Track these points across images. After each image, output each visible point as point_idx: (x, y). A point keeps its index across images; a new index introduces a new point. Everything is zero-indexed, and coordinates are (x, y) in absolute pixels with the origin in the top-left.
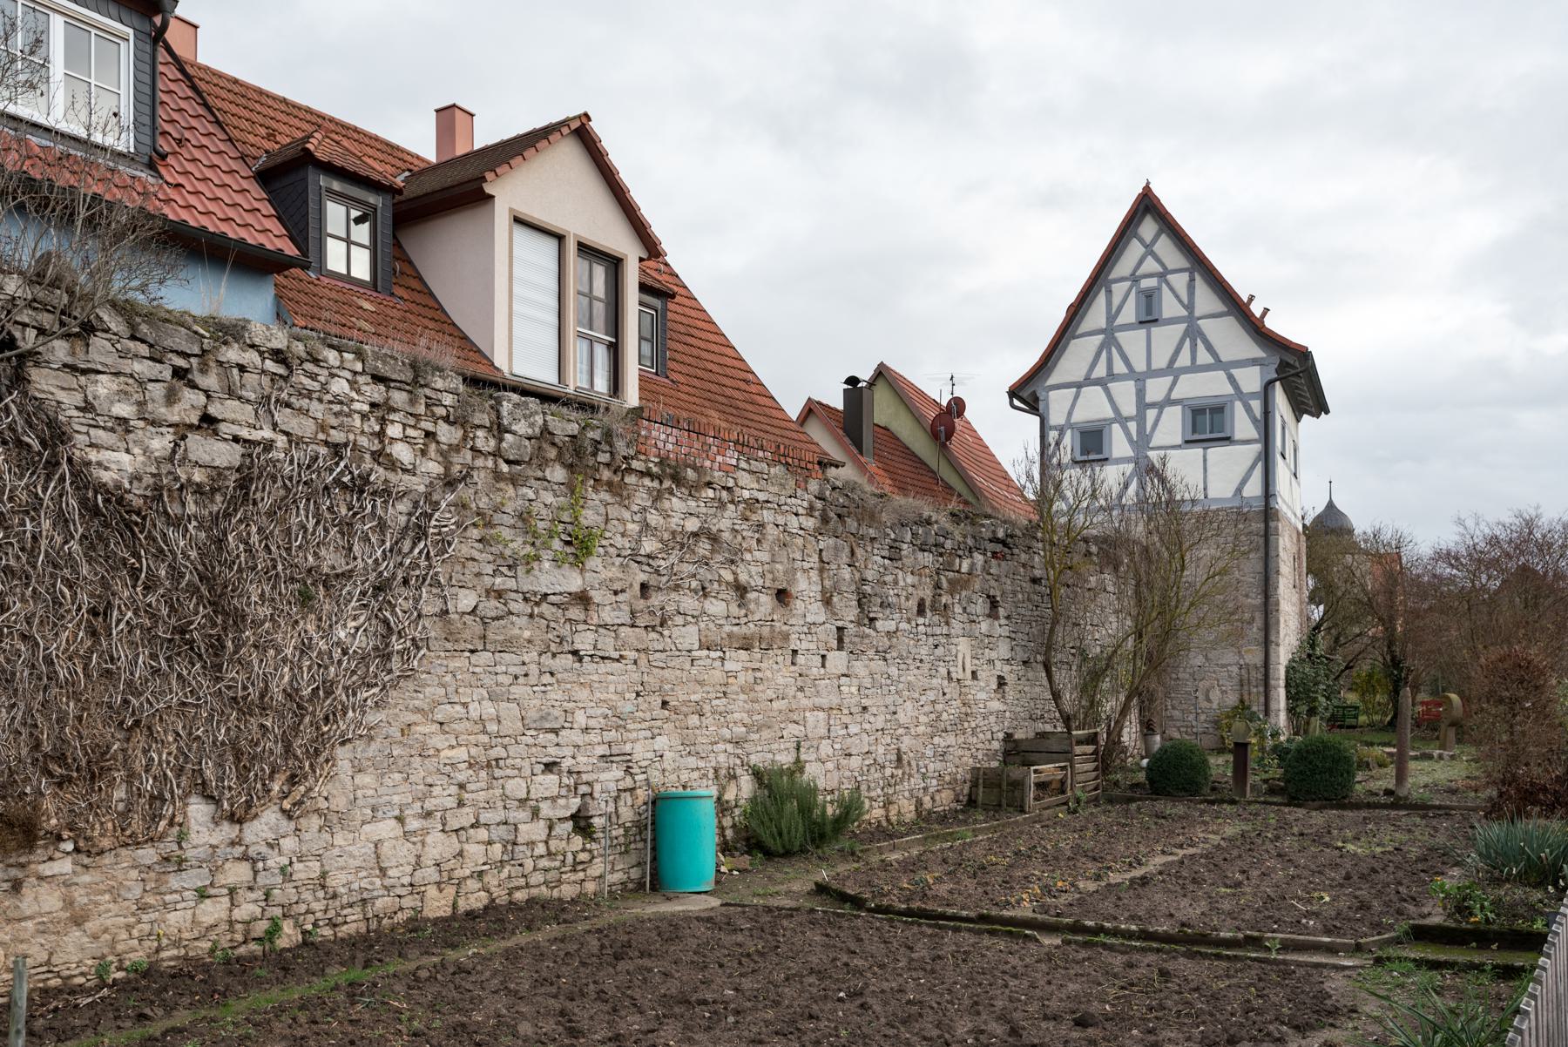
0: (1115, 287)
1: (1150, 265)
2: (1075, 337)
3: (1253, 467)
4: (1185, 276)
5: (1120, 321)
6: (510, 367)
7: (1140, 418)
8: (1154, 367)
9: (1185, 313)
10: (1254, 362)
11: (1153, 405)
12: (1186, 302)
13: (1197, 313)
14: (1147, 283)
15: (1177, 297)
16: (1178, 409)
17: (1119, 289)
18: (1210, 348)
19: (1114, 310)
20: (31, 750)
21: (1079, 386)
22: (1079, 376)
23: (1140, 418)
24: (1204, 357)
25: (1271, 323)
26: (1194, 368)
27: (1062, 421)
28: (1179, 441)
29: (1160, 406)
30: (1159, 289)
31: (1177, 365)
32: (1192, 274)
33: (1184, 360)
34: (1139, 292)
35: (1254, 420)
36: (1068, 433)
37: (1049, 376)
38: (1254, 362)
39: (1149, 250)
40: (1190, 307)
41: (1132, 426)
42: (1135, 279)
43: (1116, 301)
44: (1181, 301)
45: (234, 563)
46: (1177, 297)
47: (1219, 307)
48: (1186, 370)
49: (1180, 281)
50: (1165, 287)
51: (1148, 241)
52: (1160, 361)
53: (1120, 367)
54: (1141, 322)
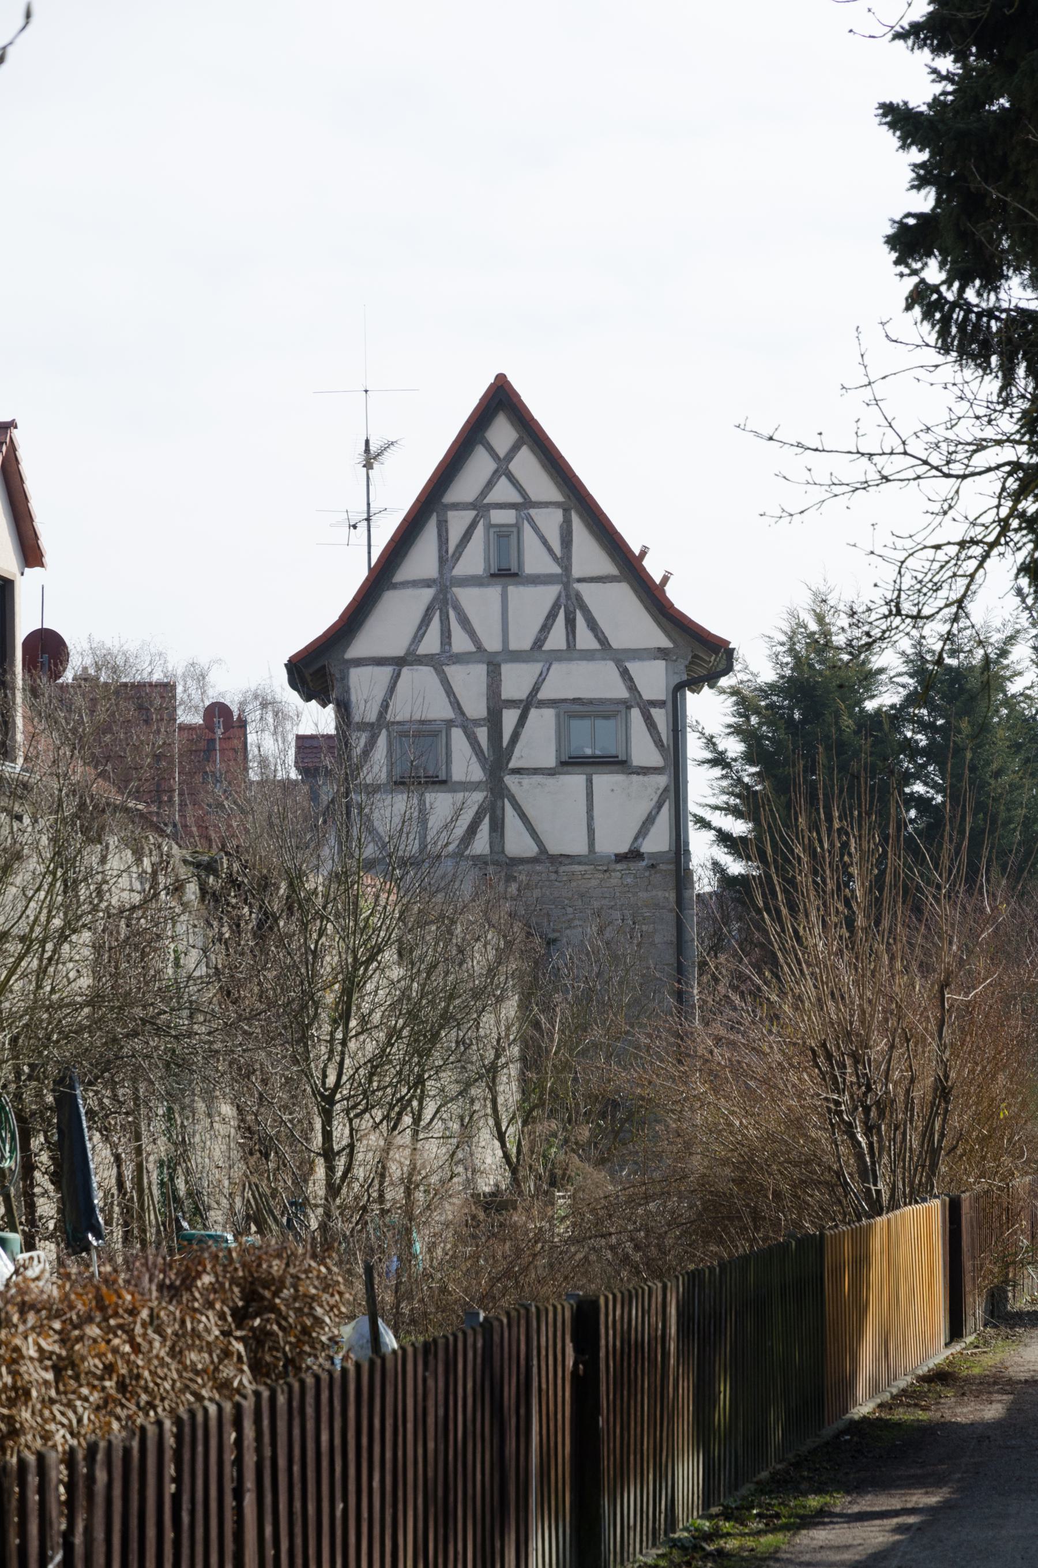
0: (451, 515)
1: (503, 491)
2: (395, 586)
3: (659, 806)
4: (558, 515)
5: (461, 569)
6: (359, 662)
7: (494, 720)
8: (513, 646)
9: (556, 570)
10: (662, 653)
11: (512, 703)
12: (559, 554)
13: (577, 572)
14: (499, 517)
15: (545, 542)
16: (549, 714)
17: (458, 523)
18: (593, 625)
19: (451, 549)
20: (241, 1317)
21: (399, 662)
22: (397, 648)
23: (494, 720)
24: (585, 639)
25: (677, 596)
26: (571, 652)
27: (372, 717)
28: (551, 762)
29: (526, 705)
30: (518, 526)
31: (547, 646)
32: (566, 511)
33: (557, 639)
34: (489, 526)
35: (658, 743)
36: (382, 741)
37: (348, 645)
38: (662, 653)
39: (503, 470)
40: (565, 561)
41: (482, 734)
42: (480, 507)
43: (454, 536)
44: (550, 550)
45: (753, 1011)
46: (545, 542)
47: (607, 567)
48: (556, 656)
49: (550, 521)
50: (527, 527)
51: (502, 452)
52: (522, 639)
53: (461, 643)
54: (493, 575)
